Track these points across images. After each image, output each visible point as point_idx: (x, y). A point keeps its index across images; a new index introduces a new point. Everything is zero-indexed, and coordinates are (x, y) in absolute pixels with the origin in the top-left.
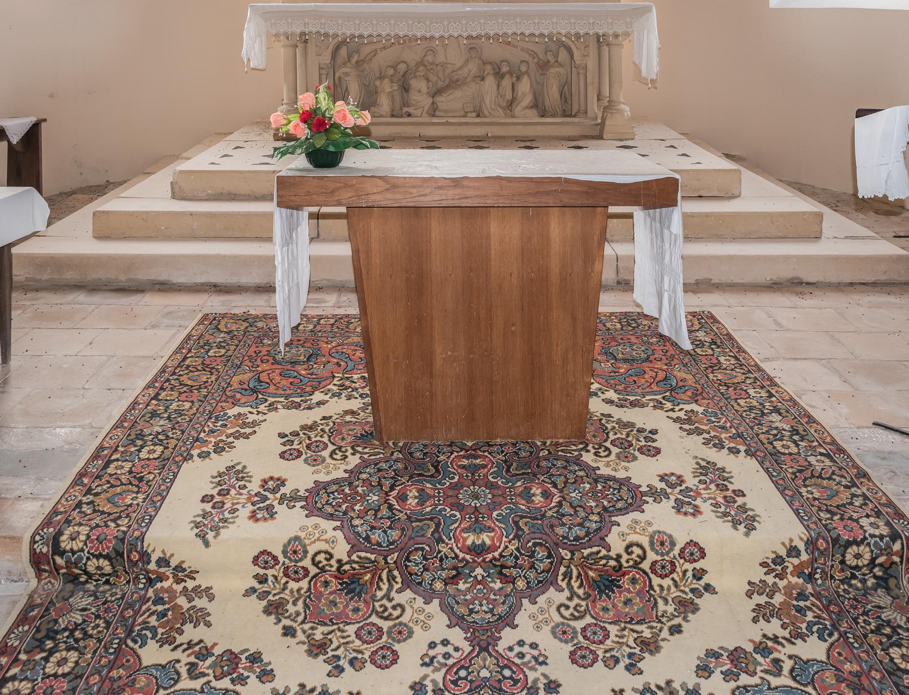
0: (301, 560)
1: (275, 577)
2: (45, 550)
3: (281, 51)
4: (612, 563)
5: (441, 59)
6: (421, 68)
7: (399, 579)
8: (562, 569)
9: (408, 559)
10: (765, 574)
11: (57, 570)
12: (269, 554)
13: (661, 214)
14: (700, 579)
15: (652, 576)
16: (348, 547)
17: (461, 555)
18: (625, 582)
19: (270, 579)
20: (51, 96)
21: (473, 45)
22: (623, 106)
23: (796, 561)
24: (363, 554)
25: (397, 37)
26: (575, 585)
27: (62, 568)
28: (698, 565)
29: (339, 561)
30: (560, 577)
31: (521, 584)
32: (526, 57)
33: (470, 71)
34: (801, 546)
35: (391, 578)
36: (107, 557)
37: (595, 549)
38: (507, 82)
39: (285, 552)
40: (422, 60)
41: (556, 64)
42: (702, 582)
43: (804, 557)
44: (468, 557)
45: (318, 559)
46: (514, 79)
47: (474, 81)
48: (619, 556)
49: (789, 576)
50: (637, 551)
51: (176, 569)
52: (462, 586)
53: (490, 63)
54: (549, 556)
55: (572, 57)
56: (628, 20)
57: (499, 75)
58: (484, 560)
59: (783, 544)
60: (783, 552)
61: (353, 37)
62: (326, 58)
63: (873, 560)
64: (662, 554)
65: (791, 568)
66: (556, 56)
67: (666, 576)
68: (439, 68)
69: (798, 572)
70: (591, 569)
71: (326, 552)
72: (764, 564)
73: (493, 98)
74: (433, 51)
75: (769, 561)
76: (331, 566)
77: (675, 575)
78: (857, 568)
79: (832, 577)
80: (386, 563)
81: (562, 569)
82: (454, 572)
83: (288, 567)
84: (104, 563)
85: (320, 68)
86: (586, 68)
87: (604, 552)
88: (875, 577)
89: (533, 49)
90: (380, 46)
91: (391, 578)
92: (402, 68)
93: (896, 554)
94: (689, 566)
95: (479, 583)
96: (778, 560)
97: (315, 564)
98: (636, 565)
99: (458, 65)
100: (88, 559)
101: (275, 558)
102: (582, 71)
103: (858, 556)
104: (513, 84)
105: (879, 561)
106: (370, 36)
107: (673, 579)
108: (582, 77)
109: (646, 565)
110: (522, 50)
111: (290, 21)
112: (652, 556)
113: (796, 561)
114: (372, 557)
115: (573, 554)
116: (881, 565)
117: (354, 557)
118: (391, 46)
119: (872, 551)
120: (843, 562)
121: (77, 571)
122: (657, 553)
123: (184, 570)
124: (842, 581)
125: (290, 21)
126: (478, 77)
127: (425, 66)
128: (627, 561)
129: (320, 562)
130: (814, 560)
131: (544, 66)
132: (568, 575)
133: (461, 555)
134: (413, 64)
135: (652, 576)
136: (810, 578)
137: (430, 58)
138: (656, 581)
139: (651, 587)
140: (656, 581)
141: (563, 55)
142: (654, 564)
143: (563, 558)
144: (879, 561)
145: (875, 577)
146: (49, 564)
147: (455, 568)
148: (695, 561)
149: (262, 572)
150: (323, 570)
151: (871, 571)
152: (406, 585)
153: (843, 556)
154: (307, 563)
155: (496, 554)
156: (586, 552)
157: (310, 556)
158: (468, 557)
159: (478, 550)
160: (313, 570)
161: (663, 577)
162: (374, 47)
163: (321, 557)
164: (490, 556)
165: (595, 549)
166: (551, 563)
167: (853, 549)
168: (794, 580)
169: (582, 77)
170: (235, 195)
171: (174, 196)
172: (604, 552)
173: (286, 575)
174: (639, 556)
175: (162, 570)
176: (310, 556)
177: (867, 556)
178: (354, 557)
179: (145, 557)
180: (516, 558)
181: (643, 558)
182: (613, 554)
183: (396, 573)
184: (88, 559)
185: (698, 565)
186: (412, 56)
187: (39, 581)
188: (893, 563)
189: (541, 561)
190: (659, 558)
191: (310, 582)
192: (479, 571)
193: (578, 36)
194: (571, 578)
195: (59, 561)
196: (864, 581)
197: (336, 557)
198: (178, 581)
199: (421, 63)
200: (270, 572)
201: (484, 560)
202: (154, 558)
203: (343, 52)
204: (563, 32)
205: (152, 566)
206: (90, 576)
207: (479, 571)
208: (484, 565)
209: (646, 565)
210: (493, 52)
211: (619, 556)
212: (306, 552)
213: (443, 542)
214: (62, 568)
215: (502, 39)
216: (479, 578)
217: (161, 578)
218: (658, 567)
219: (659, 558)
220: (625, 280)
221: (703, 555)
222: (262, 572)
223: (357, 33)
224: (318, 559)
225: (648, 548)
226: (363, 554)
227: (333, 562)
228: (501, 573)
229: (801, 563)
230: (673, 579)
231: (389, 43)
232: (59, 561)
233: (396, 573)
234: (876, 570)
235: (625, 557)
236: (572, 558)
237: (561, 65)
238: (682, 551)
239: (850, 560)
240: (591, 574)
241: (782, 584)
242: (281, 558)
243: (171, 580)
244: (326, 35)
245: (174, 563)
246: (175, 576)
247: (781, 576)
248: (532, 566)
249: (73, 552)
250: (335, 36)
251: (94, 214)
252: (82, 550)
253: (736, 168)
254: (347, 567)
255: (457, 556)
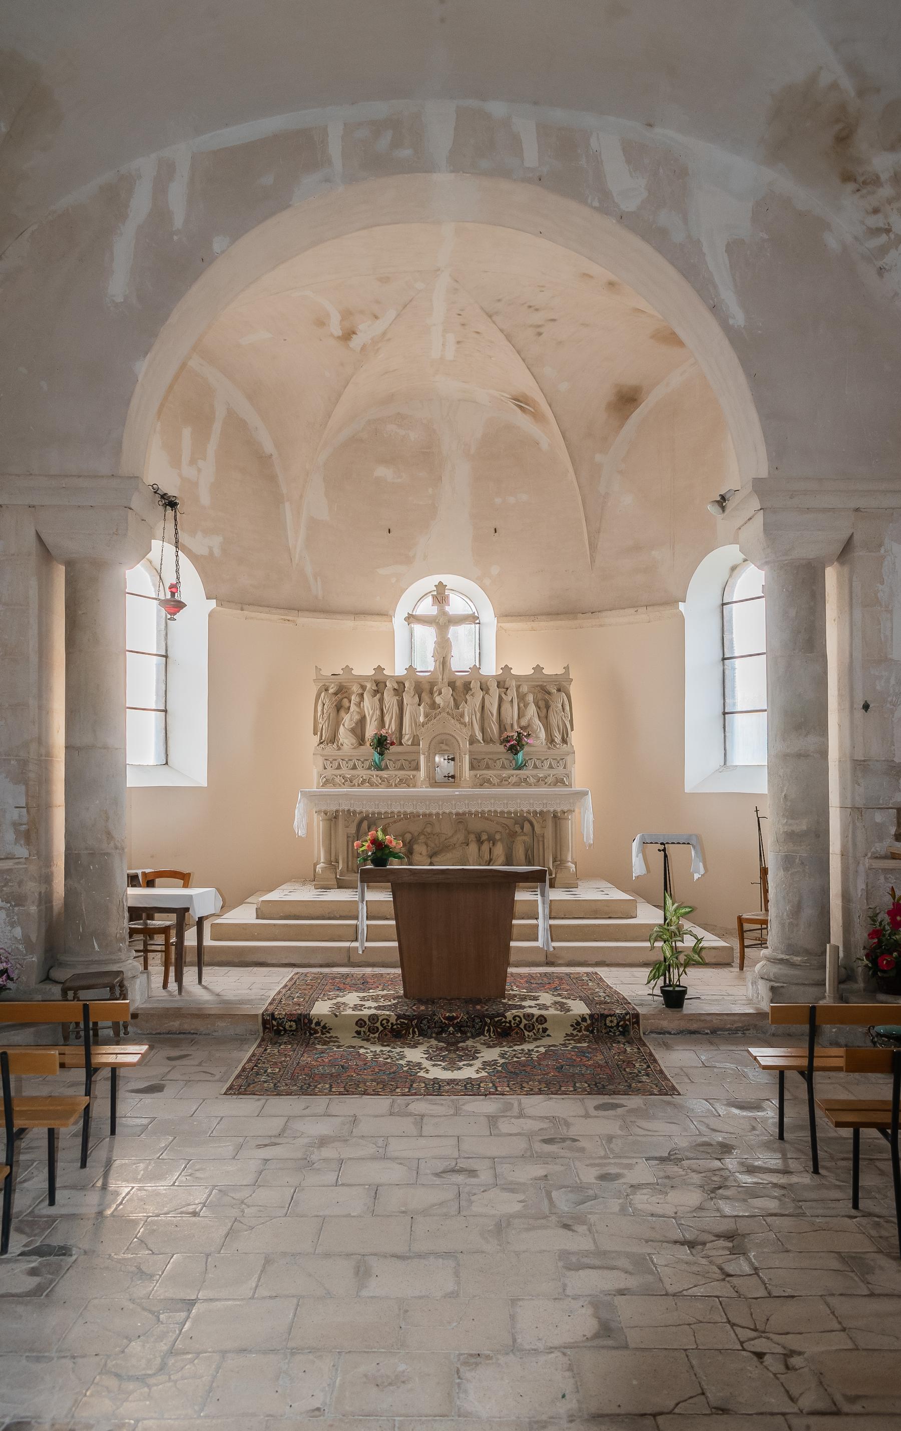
0: (376, 1023)
1: (364, 1032)
2: (268, 1018)
3: (319, 825)
4: (508, 1025)
5: (437, 830)
6: (422, 837)
7: (417, 1033)
8: (487, 1028)
9: (421, 1023)
10: (573, 1030)
11: (273, 1028)
12: (363, 1020)
13: (894, 1223)
14: (545, 1032)
15: (525, 1031)
16: (396, 1017)
17: (444, 1021)
18: (513, 1033)
19: (362, 1033)
20: (152, 857)
21: (461, 819)
22: (570, 864)
23: (585, 1024)
24: (402, 1020)
25: (405, 814)
26: (492, 1035)
27: (275, 1026)
28: (544, 1026)
29: (392, 1024)
30: (486, 1032)
31: (469, 1034)
32: (500, 829)
33: (458, 839)
34: (587, 1017)
35: (414, 1032)
36: (294, 1021)
37: (500, 1018)
38: (486, 847)
39: (369, 1019)
40: (423, 831)
41: (522, 833)
42: (546, 1034)
43: (589, 1022)
44: (446, 1022)
45: (383, 1022)
46: (491, 845)
47: (461, 846)
48: (510, 1022)
49: (583, 1031)
50: (518, 1019)
51: (322, 1027)
52: (444, 1035)
53: (473, 833)
54: (481, 1021)
55: (533, 829)
56: (571, 801)
57: (480, 842)
58: (453, 1023)
59: (580, 1016)
60: (580, 1020)
61: (373, 814)
62: (353, 830)
63: (618, 1023)
64: (529, 1021)
65: (583, 1028)
66: (522, 828)
67: (531, 1031)
68: (435, 837)
69: (587, 1029)
70: (499, 1028)
71: (387, 1019)
72: (572, 1026)
73: (475, 858)
74: (431, 824)
75: (574, 1024)
76: (389, 1026)
77: (534, 1031)
78: (612, 1027)
79: (601, 1032)
80: (412, 1024)
81: (487, 1028)
82: (441, 1029)
83: (370, 1027)
84: (293, 1024)
85: (348, 837)
86: (543, 837)
87: (504, 1020)
88: (619, 1031)
89: (505, 823)
90: (392, 820)
91: (414, 1032)
92: (408, 837)
93: (627, 1020)
94: (540, 1026)
95: (451, 1034)
96: (578, 1023)
97: (382, 1025)
98: (518, 1025)
99: (450, 834)
100: (287, 1022)
101: (365, 1022)
102: (541, 839)
103: (611, 1021)
104: (490, 849)
105: (620, 1024)
106: (386, 812)
107: (534, 1032)
108: (541, 843)
109: (522, 1026)
110: (497, 823)
111: (329, 802)
112: (524, 1022)
113: (585, 1024)
114: (406, 1022)
115: (491, 1021)
116: (621, 1026)
117: (398, 1022)
118: (400, 821)
119: (617, 1019)
120: (605, 1024)
121: (281, 1028)
122: (526, 1020)
123: (326, 1028)
124: (606, 1033)
125: (329, 802)
126: (464, 843)
127: (425, 835)
128: (514, 1024)
129: (384, 1024)
130: (592, 1024)
131: (513, 835)
132: (489, 1031)
133: (444, 1021)
134: (416, 834)
135: (525, 1031)
136: (592, 1032)
137: (429, 830)
138: (526, 1033)
139: (524, 1035)
140: (526, 1033)
141: (527, 826)
142: (525, 1025)
143: (487, 1023)
144: (620, 1024)
145: (619, 1031)
146: (270, 1024)
147: (441, 1027)
148: (543, 1024)
149: (359, 1029)
150: (385, 1028)
151: (618, 1029)
152: (420, 1035)
153: (605, 1021)
154: (378, 1024)
155: (458, 1020)
156: (496, 1019)
157: (380, 1021)
158: (446, 1022)
159: (451, 1019)
160: (381, 1028)
161: (529, 1031)
162: (388, 821)
163: (384, 1022)
164: (456, 1021)
165: (500, 1018)
166: (482, 1025)
167: (609, 1019)
168: (585, 1033)
169: (541, 843)
170: (298, 916)
171: (257, 918)
172: (504, 1020)
173: (369, 1031)
174: (518, 1021)
175: (317, 1028)
176: (380, 1021)
177: (615, 1021)
178: (398, 1022)
179: (310, 1021)
180: (467, 1022)
181: (520, 1022)
182: (508, 1020)
183: (416, 1030)
184: (287, 1022)
185: (544, 1026)
186: (415, 828)
187: (264, 1034)
188: (627, 1025)
189: (477, 1024)
190: (527, 1022)
191: (379, 1034)
192: (451, 1029)
193: (535, 812)
194: (490, 1032)
195: (274, 1023)
196: (614, 1033)
197: (391, 1022)
198: (323, 1034)
199: (422, 833)
200: (363, 1029)
201: (453, 1023)
202: (314, 1022)
203: (365, 824)
204: (525, 809)
205: (313, 1026)
206: (285, 1030)
207: (451, 1029)
208: (453, 1025)
209: (522, 1026)
210: (477, 825)
211: (510, 1022)
212: (378, 1019)
213: (436, 1015)
214: (275, 1026)
215: (483, 816)
216: (451, 1032)
217: (316, 1032)
218: (527, 1027)
219: (527, 1022)
220: (551, 962)
221: (546, 1021)
222: (359, 1029)
223: (377, 810)
224: (383, 1022)
225: (522, 1018)
226: (402, 1020)
227: (389, 1024)
228: (461, 1030)
229: (588, 1025)
230: (534, 1032)
231: (399, 818)
232: (274, 1023)
233: (416, 1030)
234: (620, 1028)
235: (513, 1022)
236: (490, 1022)
237: (525, 835)
238: (537, 1019)
239: (609, 1024)
240: (499, 1030)
241: (580, 1034)
242: (367, 1022)
243: (320, 1034)
244: (354, 812)
245: (322, 1024)
246: (322, 1031)
247: (580, 1031)
248: (474, 1027)
249: (280, 1019)
250: (361, 812)
251: (211, 925)
252: (284, 1018)
253: (632, 898)
254: (395, 1027)
255: (442, 1021)
